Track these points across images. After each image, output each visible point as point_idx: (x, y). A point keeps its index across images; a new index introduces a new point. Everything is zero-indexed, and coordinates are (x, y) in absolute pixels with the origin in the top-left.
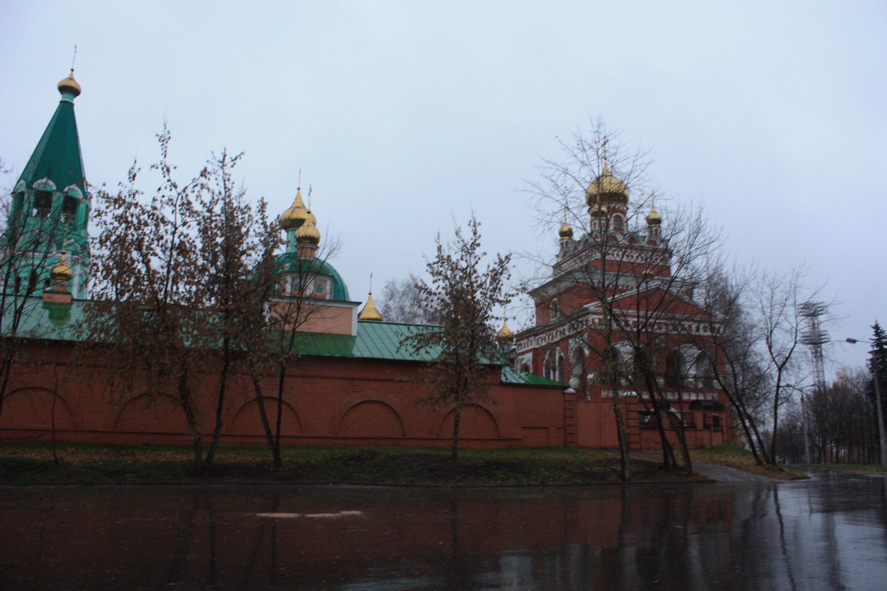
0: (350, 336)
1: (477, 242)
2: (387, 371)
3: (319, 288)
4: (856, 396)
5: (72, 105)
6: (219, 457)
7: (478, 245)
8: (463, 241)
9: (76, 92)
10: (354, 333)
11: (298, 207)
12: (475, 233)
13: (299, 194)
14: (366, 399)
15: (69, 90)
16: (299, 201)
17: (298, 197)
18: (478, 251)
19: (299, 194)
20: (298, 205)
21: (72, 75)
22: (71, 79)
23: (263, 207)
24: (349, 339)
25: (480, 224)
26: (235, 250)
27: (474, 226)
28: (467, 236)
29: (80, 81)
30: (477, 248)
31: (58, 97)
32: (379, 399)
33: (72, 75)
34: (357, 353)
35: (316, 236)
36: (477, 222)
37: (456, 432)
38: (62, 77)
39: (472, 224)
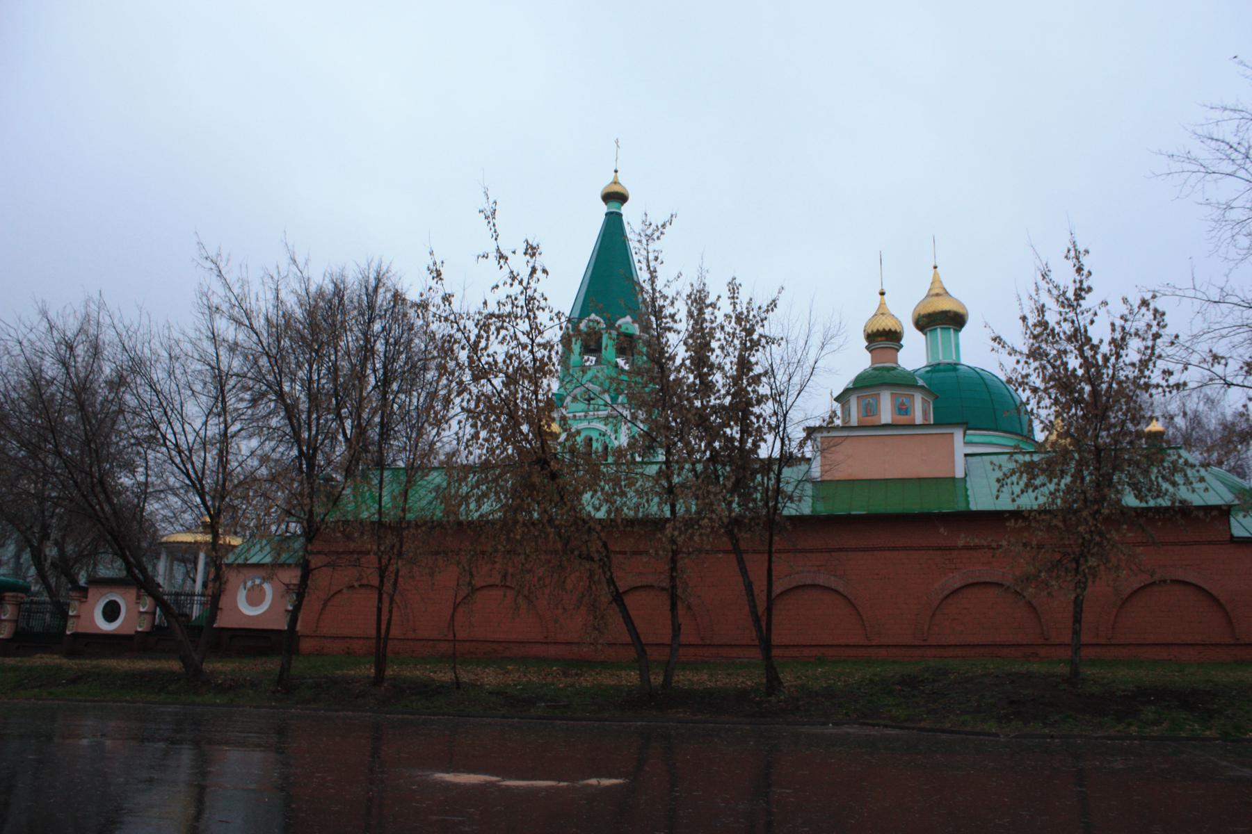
0: (954, 479)
1: (1085, 285)
2: (942, 530)
3: (902, 409)
4: (515, 411)
5: (620, 215)
6: (684, 679)
7: (1090, 289)
8: (1057, 287)
9: (621, 198)
10: (959, 474)
11: (937, 295)
12: (1079, 270)
13: (936, 275)
14: (971, 581)
15: (615, 197)
16: (937, 284)
17: (936, 280)
18: (1089, 302)
19: (936, 275)
20: (938, 292)
21: (616, 177)
22: (615, 183)
23: (734, 289)
24: (952, 484)
25: (1087, 252)
26: (749, 362)
27: (1077, 258)
28: (1065, 277)
29: (628, 184)
30: (1088, 296)
31: (603, 209)
32: (994, 580)
33: (616, 177)
34: (973, 507)
35: (896, 332)
36: (1081, 249)
37: (1076, 633)
38: (603, 183)
39: (1072, 254)
